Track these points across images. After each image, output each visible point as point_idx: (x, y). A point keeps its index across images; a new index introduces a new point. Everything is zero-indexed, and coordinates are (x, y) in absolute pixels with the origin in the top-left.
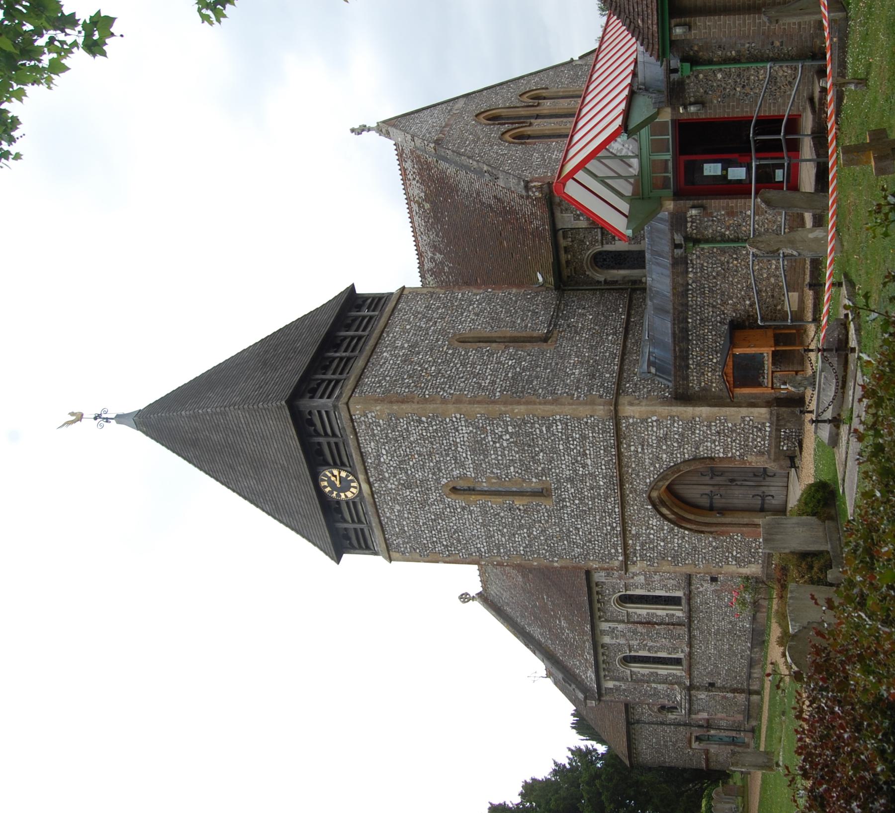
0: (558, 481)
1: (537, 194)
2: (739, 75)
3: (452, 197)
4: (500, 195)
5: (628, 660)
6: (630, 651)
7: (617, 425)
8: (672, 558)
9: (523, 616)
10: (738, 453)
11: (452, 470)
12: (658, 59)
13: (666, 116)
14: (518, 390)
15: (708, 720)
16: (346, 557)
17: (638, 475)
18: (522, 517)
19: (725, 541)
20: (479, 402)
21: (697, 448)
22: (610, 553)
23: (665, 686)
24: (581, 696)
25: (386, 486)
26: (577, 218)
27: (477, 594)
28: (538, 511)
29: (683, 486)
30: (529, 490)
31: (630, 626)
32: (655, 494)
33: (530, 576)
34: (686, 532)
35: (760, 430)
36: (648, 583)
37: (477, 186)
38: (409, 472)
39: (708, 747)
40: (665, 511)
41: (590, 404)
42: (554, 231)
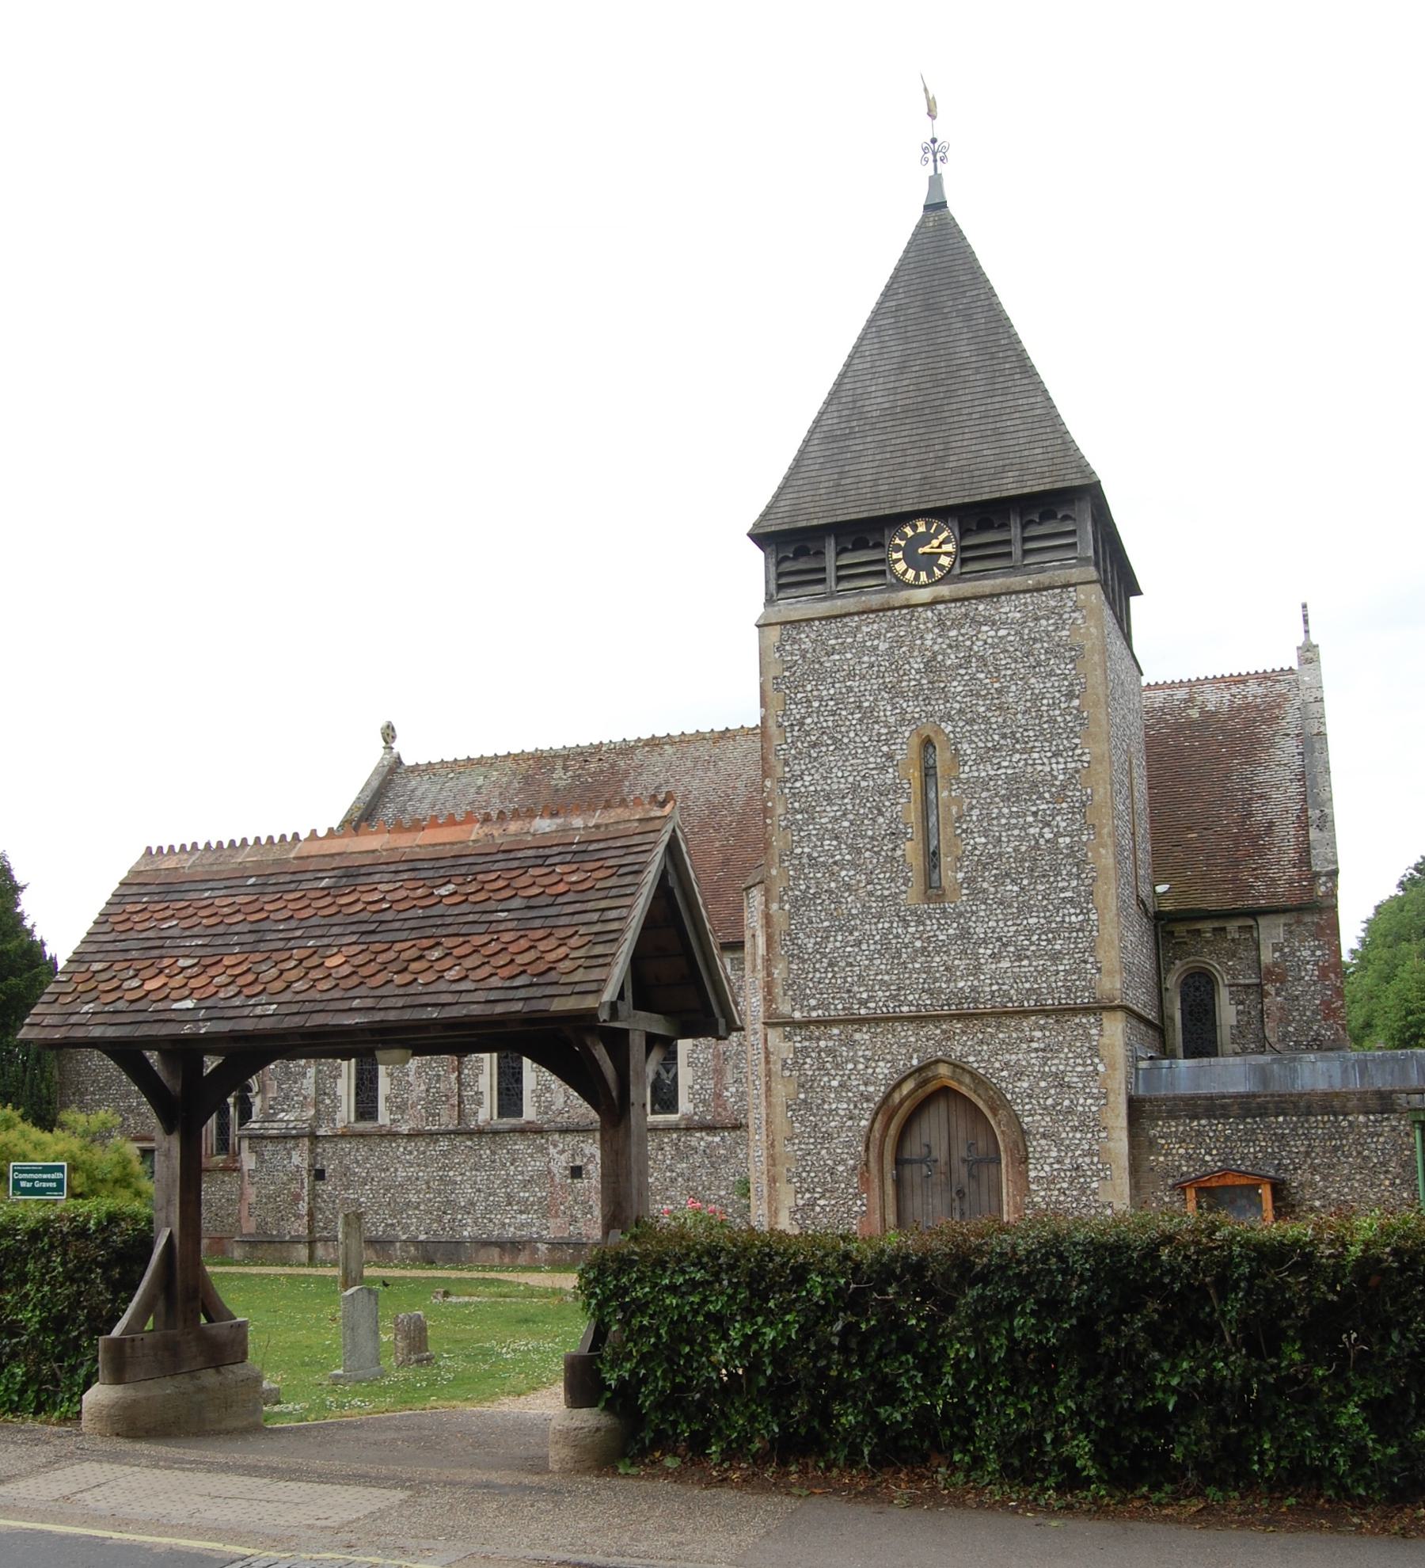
0: (961, 915)
1: (1323, 889)
3: (1233, 755)
4: (1279, 831)
7: (1086, 1010)
8: (805, 1101)
11: (973, 742)
17: (981, 1042)
18: (878, 853)
21: (1044, 1136)
22: (806, 997)
23: (311, 1091)
25: (928, 630)
26: (1277, 948)
32: (943, 1070)
38: (963, 672)
40: (907, 1088)
42: (1255, 913)
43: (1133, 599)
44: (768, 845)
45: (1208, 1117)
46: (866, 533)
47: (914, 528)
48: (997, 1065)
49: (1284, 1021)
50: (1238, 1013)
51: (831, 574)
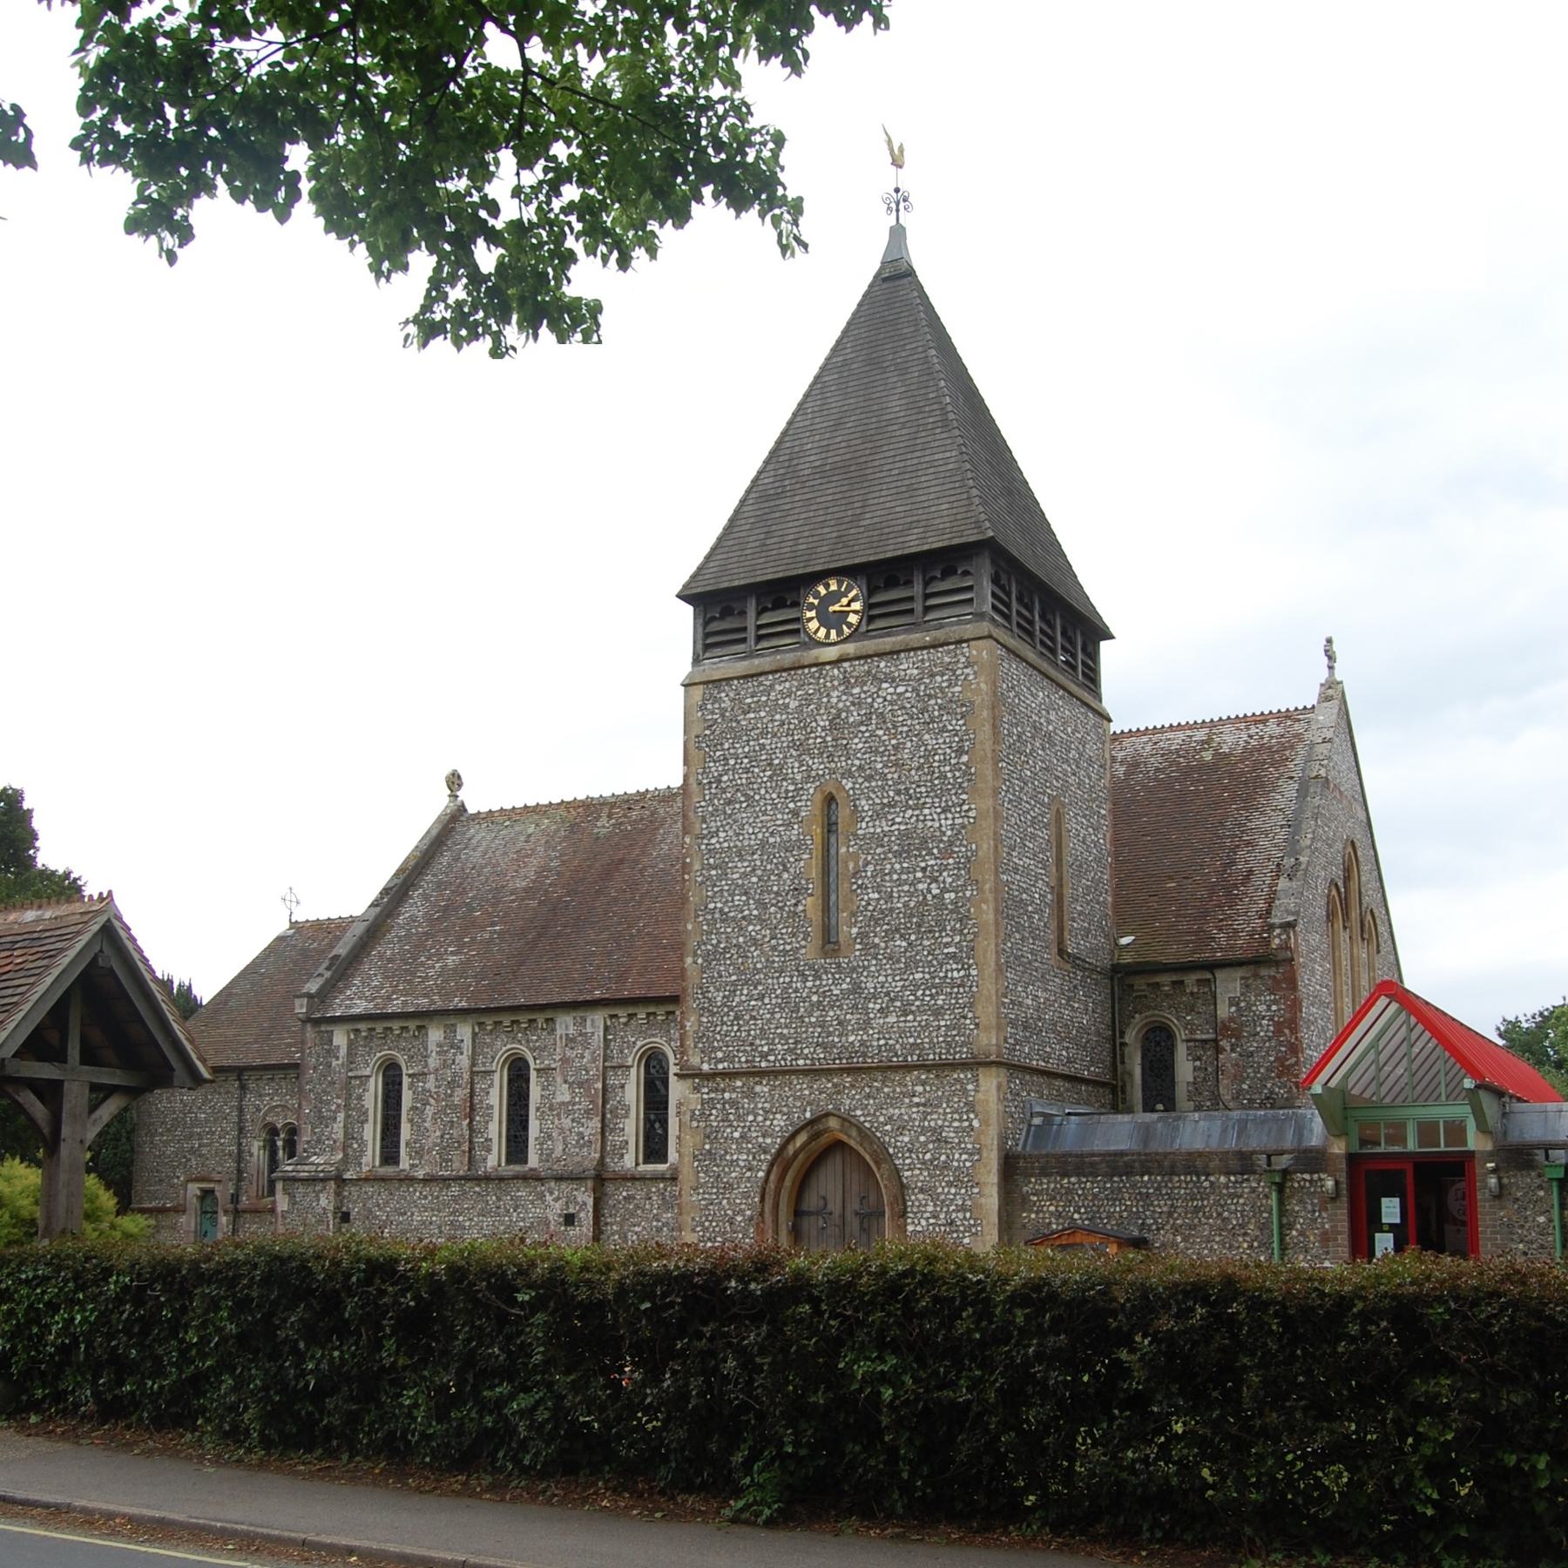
0: (854, 969)
2: (1542, 1246)
3: (1233, 800)
4: (1256, 881)
5: (391, 1073)
6: (410, 1076)
7: (963, 1065)
8: (709, 1151)
9: (440, 886)
13: (1475, 1142)
14: (1010, 907)
15: (273, 1211)
16: (688, 610)
17: (868, 1096)
21: (922, 1190)
22: (715, 1050)
23: (340, 1135)
24: (313, 987)
25: (834, 688)
26: (1233, 1002)
29: (839, 1173)
31: (466, 1076)
32: (833, 1123)
34: (761, 1174)
36: (550, 1108)
37: (1263, 842)
40: (801, 1140)
42: (1212, 966)
43: (1103, 644)
44: (684, 899)
45: (1078, 1175)
46: (783, 593)
47: (827, 586)
48: (882, 1119)
49: (1238, 1078)
50: (1195, 1069)
51: (751, 634)
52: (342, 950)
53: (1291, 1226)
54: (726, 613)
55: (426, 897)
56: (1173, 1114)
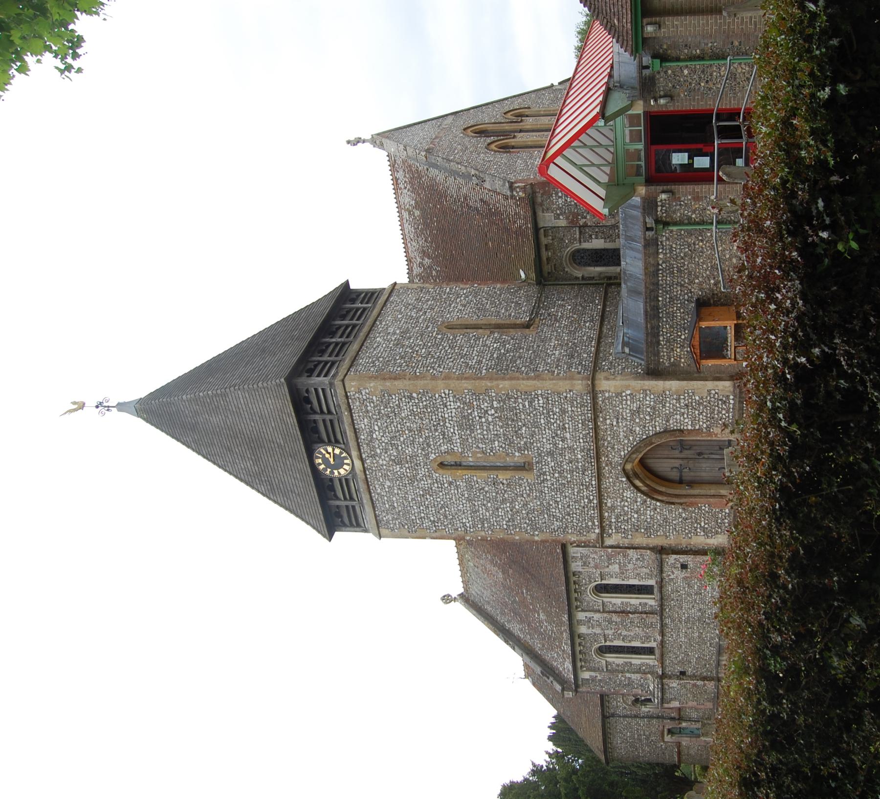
0: (540, 455)
2: (703, 72)
3: (441, 203)
4: (486, 198)
5: (603, 650)
6: (605, 641)
7: (594, 398)
10: (705, 426)
12: (631, 54)
13: (639, 109)
14: (502, 368)
15: (679, 709)
16: (337, 534)
17: (613, 448)
18: (505, 491)
19: (693, 512)
20: (466, 379)
21: (668, 421)
22: (587, 526)
23: (638, 676)
24: (558, 688)
26: (557, 217)
27: (459, 595)
28: (520, 485)
30: (512, 464)
31: (605, 615)
32: (629, 467)
33: (511, 571)
34: (658, 504)
35: (725, 402)
36: (622, 573)
39: (680, 739)
40: (638, 483)
41: (569, 379)
42: (536, 229)
45: (658, 336)
46: (325, 487)
47: (320, 464)
48: (626, 441)
52: (538, 670)
53: (690, 218)
54: (339, 515)
55: (509, 621)
56: (622, 275)
